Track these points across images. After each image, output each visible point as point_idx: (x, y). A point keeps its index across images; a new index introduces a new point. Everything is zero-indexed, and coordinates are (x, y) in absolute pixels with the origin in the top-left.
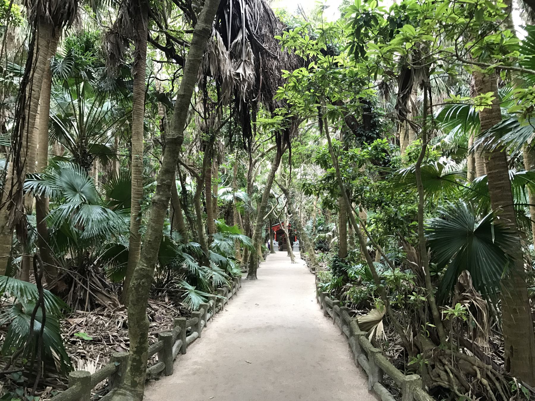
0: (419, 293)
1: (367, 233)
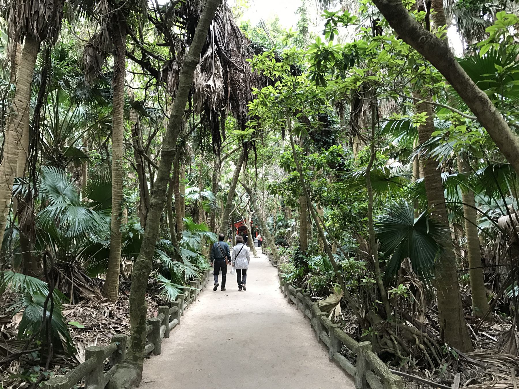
0: (370, 277)
1: (325, 227)
